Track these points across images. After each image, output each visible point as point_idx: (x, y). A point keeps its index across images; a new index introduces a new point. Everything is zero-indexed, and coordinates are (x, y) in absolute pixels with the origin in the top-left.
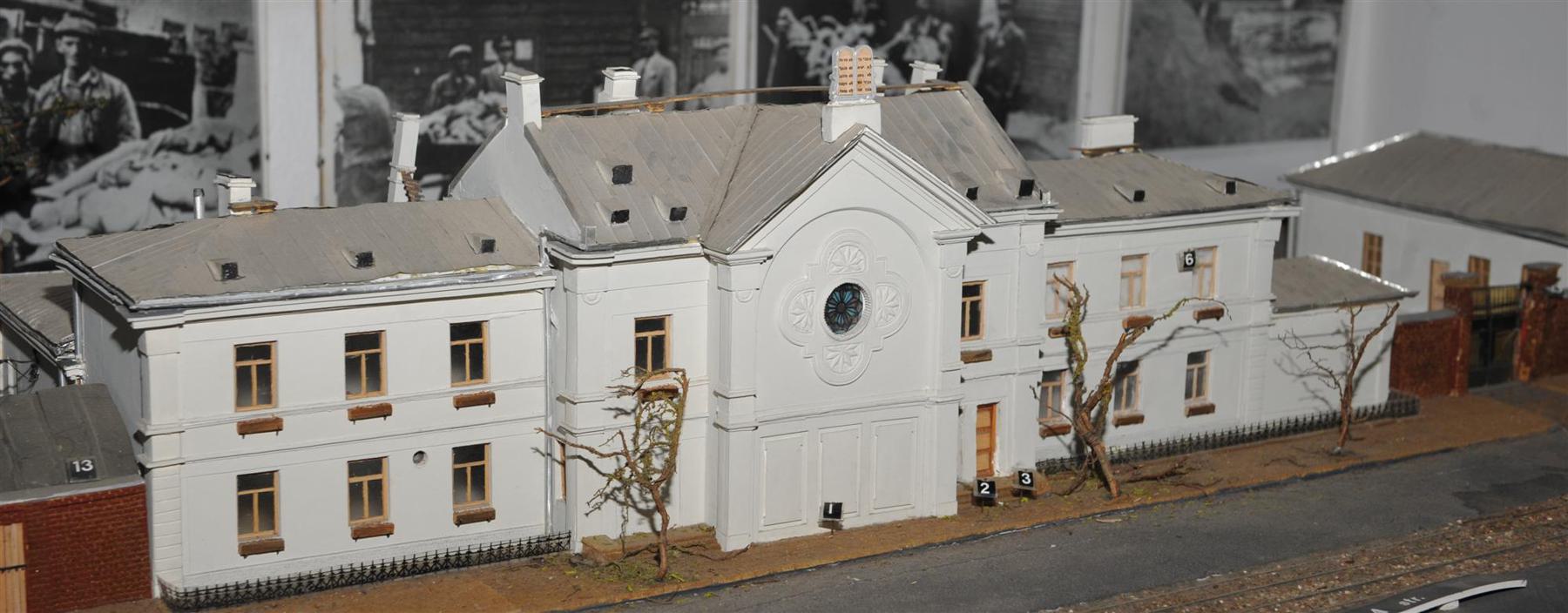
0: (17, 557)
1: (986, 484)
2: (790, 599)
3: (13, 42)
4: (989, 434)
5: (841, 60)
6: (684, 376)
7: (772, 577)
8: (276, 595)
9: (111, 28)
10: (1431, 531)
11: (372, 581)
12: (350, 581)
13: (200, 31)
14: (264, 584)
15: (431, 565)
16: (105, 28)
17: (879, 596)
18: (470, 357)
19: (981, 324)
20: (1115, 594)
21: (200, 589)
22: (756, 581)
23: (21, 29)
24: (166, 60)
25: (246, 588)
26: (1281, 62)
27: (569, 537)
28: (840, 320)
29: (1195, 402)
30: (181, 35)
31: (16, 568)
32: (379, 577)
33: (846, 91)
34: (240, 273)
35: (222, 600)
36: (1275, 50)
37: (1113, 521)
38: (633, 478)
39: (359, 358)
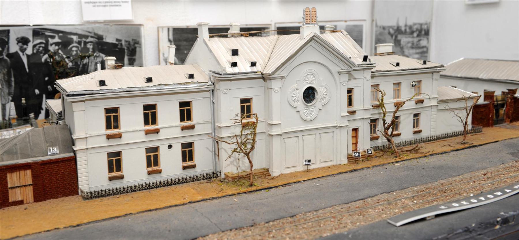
0: (29, 181)
1: (357, 153)
2: (295, 191)
3: (75, 44)
4: (355, 138)
5: (306, 11)
6: (256, 116)
7: (288, 184)
8: (119, 193)
9: (102, 41)
10: (507, 165)
11: (153, 188)
12: (145, 188)
13: (126, 41)
14: (115, 189)
15: (173, 182)
16: (100, 41)
17: (326, 190)
18: (186, 113)
19: (352, 103)
20: (409, 187)
21: (102, 190)
22: (283, 186)
23: (77, 41)
24: (117, 49)
25: (109, 191)
26: (414, 51)
27: (220, 172)
28: (308, 99)
29: (416, 129)
30: (121, 43)
31: (29, 185)
32: (155, 187)
33: (308, 22)
34: (106, 83)
35: (100, 195)
36: (412, 48)
37: (399, 164)
38: (241, 151)
39: (149, 113)
